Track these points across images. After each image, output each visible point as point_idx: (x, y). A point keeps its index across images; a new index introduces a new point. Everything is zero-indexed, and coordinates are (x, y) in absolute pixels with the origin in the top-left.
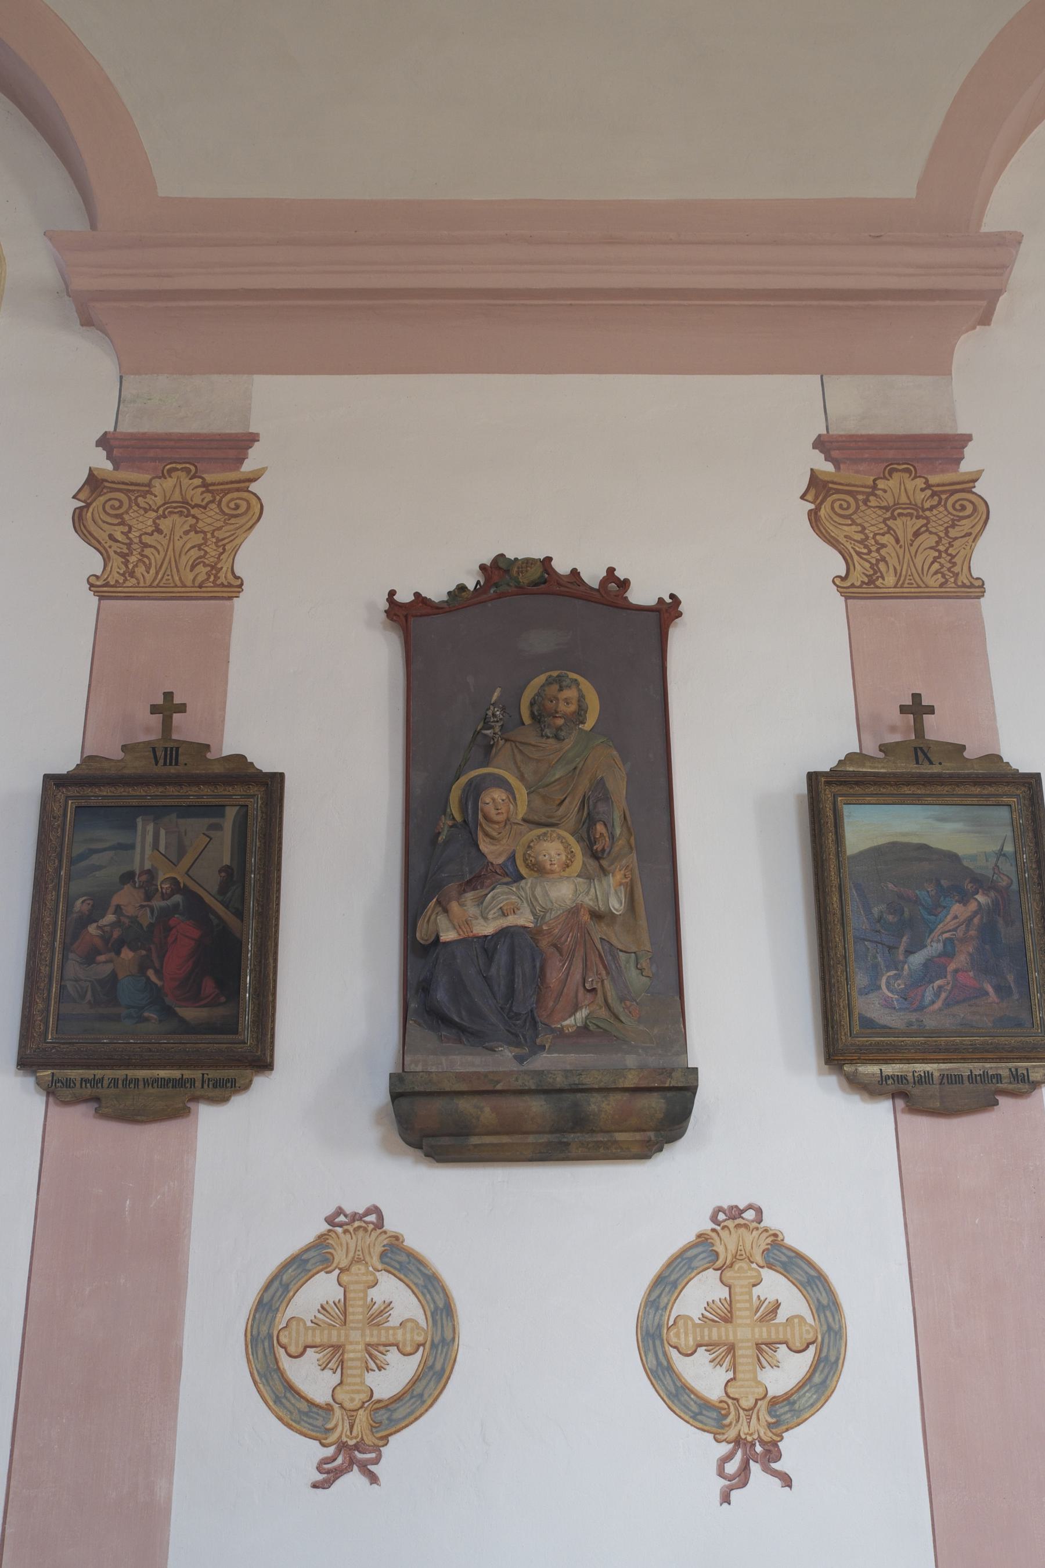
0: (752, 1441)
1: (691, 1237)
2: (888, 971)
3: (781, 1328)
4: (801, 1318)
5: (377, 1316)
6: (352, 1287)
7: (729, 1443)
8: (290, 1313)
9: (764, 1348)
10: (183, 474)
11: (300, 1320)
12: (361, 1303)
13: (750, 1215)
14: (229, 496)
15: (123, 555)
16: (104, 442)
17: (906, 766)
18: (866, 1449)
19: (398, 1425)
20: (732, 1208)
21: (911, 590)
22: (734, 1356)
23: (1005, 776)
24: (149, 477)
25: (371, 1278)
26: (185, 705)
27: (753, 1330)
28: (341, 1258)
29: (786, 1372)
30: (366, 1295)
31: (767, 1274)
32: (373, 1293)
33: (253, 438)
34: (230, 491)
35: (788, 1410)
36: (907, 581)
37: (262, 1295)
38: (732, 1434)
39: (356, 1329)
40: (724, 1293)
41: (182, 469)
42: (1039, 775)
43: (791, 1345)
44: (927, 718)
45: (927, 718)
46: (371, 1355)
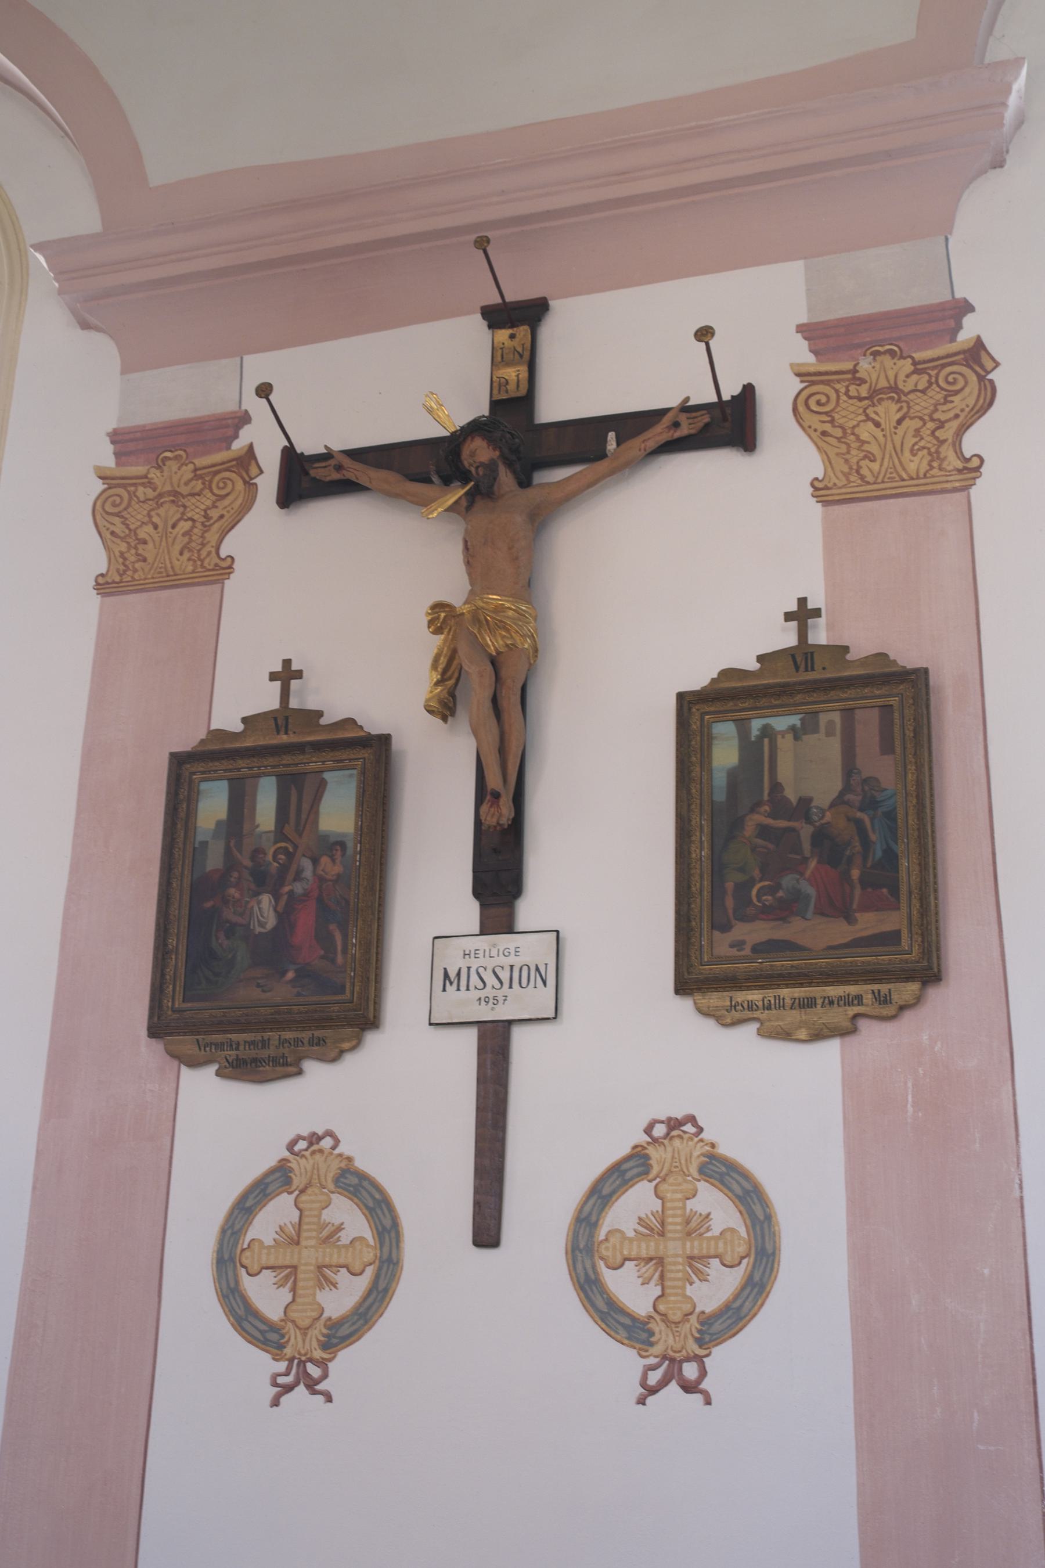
0: (676, 1353)
1: (625, 1150)
2: (761, 880)
3: (713, 1243)
4: (732, 1230)
5: (331, 1236)
6: (306, 1213)
7: (656, 1357)
8: (250, 1235)
9: (696, 1263)
10: (887, 357)
11: (261, 1242)
12: (679, 1212)
13: (327, 1143)
14: (217, 478)
15: (864, 442)
16: (117, 437)
17: (786, 676)
18: (797, 1360)
19: (719, 1339)
20: (670, 1119)
21: (170, 581)
22: (295, 1282)
23: (893, 674)
24: (147, 468)
25: (690, 1187)
26: (799, 600)
27: (684, 1245)
28: (298, 1181)
29: (341, 1298)
30: (684, 1207)
31: (703, 1186)
32: (690, 1204)
33: (966, 307)
34: (944, 366)
35: (341, 1334)
36: (888, 475)
37: (582, 1207)
38: (658, 1349)
39: (674, 1239)
40: (657, 1205)
41: (885, 353)
42: (681, 696)
43: (351, 1269)
44: (294, 684)
45: (294, 684)
46: (691, 1266)
